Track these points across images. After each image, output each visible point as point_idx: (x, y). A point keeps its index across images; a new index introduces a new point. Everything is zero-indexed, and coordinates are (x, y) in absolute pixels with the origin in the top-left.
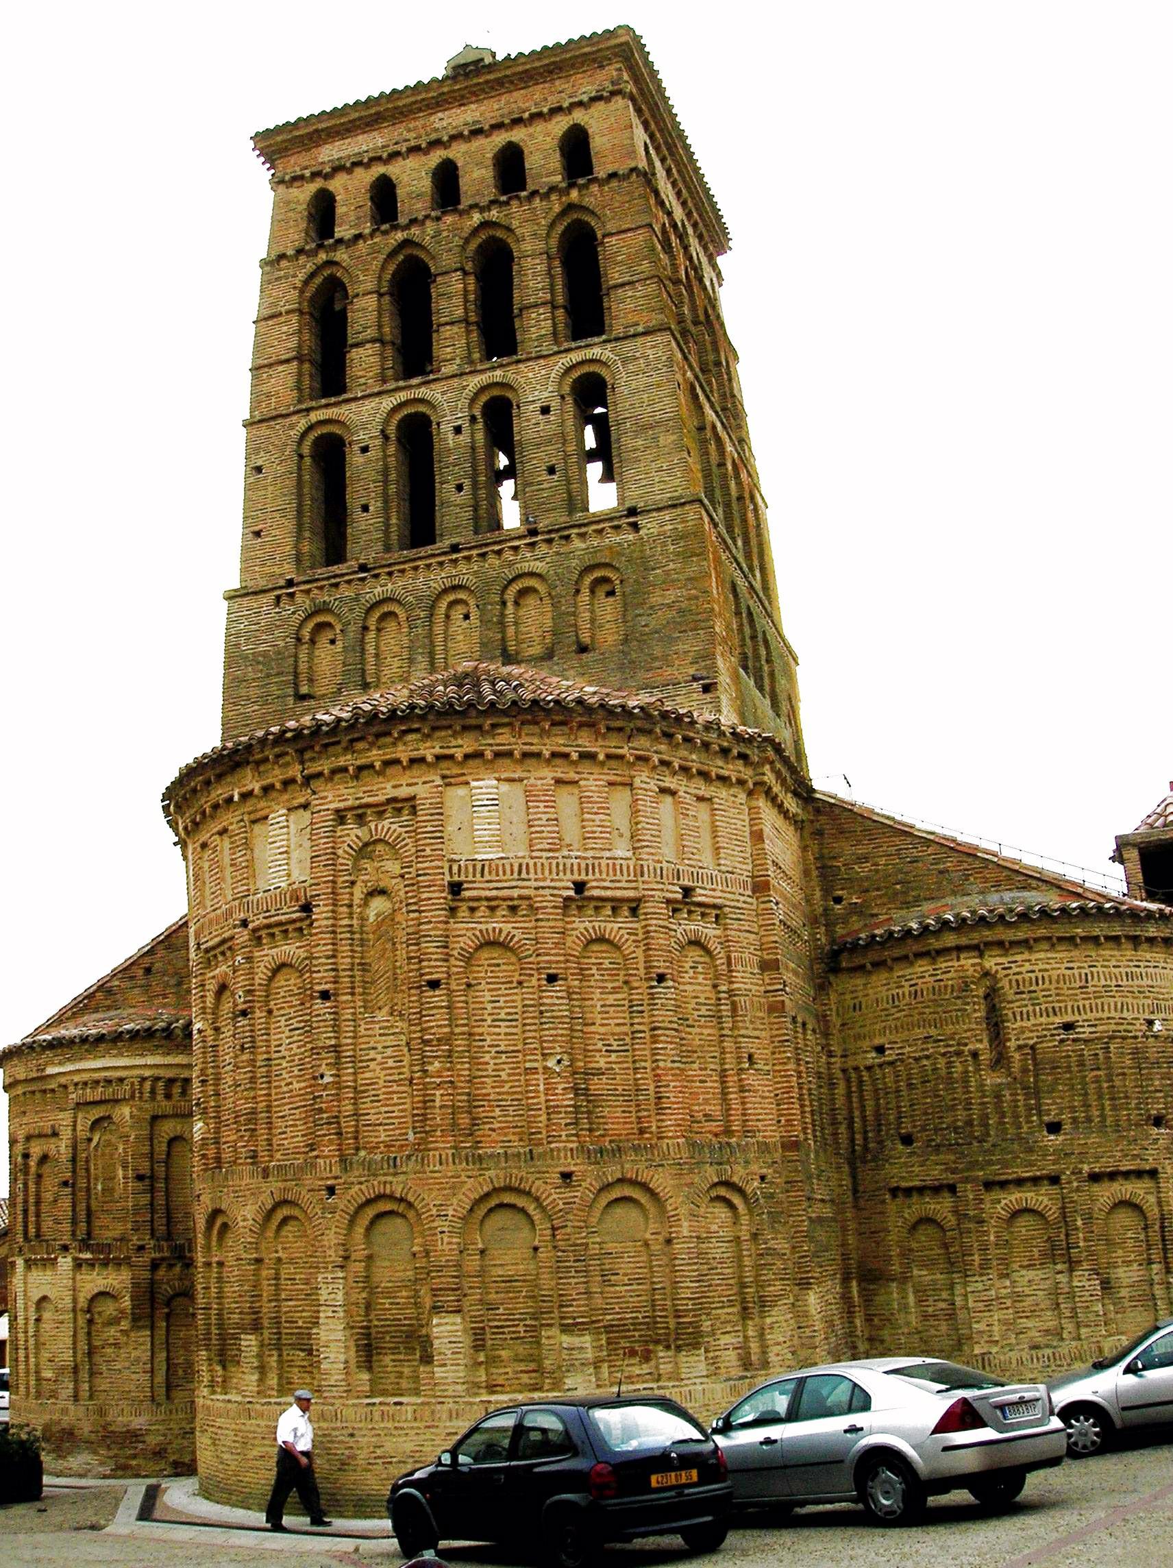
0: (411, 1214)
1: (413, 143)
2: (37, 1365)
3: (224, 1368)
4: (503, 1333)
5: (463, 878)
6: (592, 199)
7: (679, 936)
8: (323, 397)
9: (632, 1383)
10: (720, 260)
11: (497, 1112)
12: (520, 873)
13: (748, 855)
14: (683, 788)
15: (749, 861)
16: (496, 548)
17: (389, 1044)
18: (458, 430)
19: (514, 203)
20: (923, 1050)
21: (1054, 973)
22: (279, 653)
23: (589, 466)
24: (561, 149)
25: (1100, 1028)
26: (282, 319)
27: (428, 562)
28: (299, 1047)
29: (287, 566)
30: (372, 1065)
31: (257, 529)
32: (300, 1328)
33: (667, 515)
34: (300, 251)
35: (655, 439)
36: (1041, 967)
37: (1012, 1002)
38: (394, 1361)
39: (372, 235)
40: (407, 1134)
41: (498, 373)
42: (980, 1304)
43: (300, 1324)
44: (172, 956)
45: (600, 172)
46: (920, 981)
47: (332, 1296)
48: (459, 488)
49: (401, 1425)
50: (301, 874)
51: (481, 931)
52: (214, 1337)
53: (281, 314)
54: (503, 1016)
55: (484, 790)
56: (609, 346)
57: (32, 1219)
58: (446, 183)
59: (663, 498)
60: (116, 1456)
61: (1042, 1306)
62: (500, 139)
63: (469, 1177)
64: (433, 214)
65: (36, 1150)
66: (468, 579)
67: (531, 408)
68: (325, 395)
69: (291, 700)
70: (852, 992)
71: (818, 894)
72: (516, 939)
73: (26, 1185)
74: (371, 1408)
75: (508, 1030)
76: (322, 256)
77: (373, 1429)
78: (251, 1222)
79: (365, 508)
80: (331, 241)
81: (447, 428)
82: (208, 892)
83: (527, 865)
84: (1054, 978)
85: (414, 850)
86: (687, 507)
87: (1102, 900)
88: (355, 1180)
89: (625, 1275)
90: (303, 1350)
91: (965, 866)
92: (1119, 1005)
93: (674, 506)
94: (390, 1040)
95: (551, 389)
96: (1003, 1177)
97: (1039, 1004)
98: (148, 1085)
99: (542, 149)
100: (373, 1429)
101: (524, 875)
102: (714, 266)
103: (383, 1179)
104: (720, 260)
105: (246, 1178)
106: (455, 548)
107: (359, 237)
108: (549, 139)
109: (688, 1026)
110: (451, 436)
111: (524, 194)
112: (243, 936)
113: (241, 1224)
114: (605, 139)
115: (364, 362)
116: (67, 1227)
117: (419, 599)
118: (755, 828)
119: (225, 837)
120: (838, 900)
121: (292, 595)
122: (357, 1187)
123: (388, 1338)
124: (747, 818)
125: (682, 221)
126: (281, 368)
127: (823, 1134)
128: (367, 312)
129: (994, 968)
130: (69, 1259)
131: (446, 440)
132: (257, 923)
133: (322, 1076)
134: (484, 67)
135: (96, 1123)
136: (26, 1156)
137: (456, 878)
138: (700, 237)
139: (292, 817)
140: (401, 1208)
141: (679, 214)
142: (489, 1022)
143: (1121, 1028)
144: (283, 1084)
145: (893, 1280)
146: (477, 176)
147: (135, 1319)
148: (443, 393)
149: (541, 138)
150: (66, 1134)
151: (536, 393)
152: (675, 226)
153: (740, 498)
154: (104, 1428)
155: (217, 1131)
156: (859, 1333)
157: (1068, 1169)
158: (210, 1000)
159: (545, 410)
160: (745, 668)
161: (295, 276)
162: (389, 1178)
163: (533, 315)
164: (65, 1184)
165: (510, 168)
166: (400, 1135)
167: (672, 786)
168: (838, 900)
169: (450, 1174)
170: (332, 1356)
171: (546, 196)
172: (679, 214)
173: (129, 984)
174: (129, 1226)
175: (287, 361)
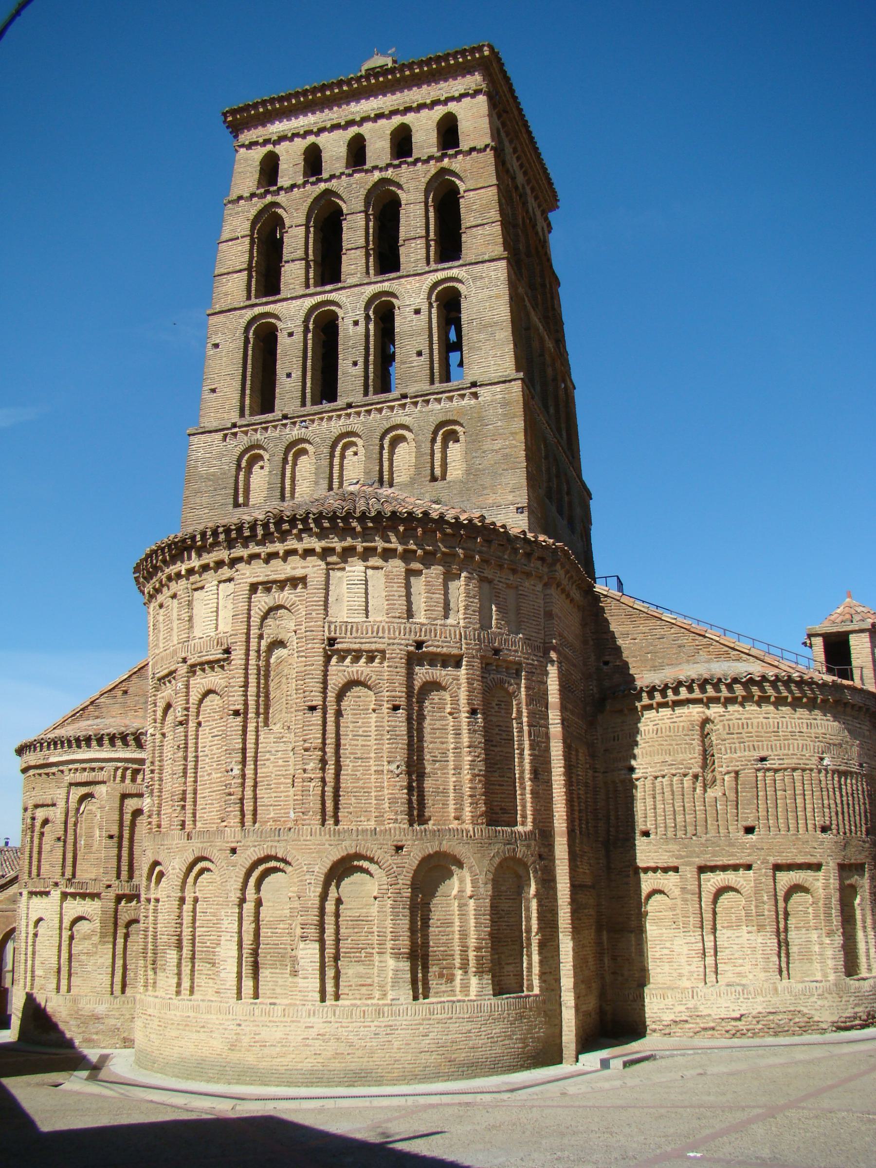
0: (289, 869)
1: (335, 122)
2: (33, 966)
3: (155, 973)
4: (350, 957)
5: (338, 635)
6: (458, 165)
7: (489, 682)
8: (266, 296)
9: (440, 997)
10: (551, 216)
11: (353, 800)
12: (377, 633)
13: (542, 628)
14: (498, 579)
15: (543, 632)
16: (378, 406)
17: (279, 749)
18: (356, 323)
19: (404, 166)
20: (661, 770)
21: (755, 721)
22: (225, 474)
23: (450, 354)
24: (438, 129)
25: (786, 761)
26: (239, 241)
27: (330, 414)
28: (218, 749)
29: (233, 414)
30: (267, 763)
31: (213, 387)
32: (208, 947)
33: (498, 388)
34: (253, 195)
35: (493, 334)
36: (747, 716)
37: (725, 740)
38: (272, 973)
39: (305, 183)
40: (289, 813)
41: (386, 284)
42: (693, 952)
43: (208, 944)
44: (141, 683)
45: (464, 146)
46: (660, 722)
47: (231, 925)
48: (355, 364)
49: (273, 1019)
50: (225, 626)
51: (348, 672)
52: (149, 951)
53: (238, 238)
54: (361, 733)
55: (356, 574)
56: (464, 268)
57: (35, 863)
58: (357, 153)
59: (494, 376)
60: (84, 1032)
61: (736, 956)
62: (397, 120)
63: (331, 845)
64: (347, 171)
65: (41, 814)
66: (357, 428)
67: (408, 310)
68: (266, 295)
69: (231, 507)
70: (613, 728)
71: (593, 658)
72: (373, 679)
73: (32, 837)
74: (253, 1006)
75: (364, 743)
76: (269, 198)
77: (254, 1021)
78: (178, 870)
79: (289, 375)
80: (275, 188)
81: (349, 322)
82: (161, 638)
83: (383, 627)
84: (755, 724)
85: (304, 613)
86: (513, 383)
87: (792, 671)
88: (251, 844)
89: (438, 920)
90: (210, 963)
91: (697, 643)
92: (800, 746)
93: (504, 382)
94: (282, 746)
95: (422, 297)
96: (712, 863)
97: (744, 742)
98: (119, 772)
99: (424, 129)
100: (254, 1021)
101: (380, 634)
102: (546, 219)
103: (270, 844)
104: (551, 216)
105: (176, 839)
106: (349, 406)
107: (293, 186)
108: (430, 122)
109: (492, 746)
110: (351, 327)
111: (410, 160)
112: (183, 669)
113: (171, 872)
114: (469, 123)
115: (293, 273)
116: (59, 870)
117: (324, 440)
118: (547, 609)
119: (175, 601)
120: (606, 663)
121: (235, 434)
122: (253, 849)
123: (269, 958)
124: (542, 602)
125: (523, 185)
126: (235, 275)
127: (587, 827)
128: (296, 240)
129: (713, 715)
130: (59, 892)
131: (347, 329)
132: (193, 660)
133: (232, 770)
134: (386, 69)
135: (83, 798)
136: (33, 819)
137: (333, 634)
138: (536, 198)
139: (222, 586)
140: (282, 865)
141: (520, 179)
142: (350, 737)
143: (801, 761)
144: (205, 774)
145: (631, 932)
146: (379, 147)
147: (103, 935)
148: (348, 297)
149: (424, 121)
150: (61, 804)
151: (412, 299)
152: (516, 188)
153: (555, 379)
154: (77, 1012)
155: (160, 806)
156: (606, 968)
157: (759, 859)
158: (159, 713)
159: (417, 312)
160: (550, 498)
161: (248, 211)
162: (275, 844)
163: (413, 245)
164: (59, 839)
165: (402, 144)
166: (285, 813)
167: (490, 577)
168: (606, 663)
169: (317, 842)
170: (228, 967)
171: (427, 161)
172: (520, 179)
173: (111, 701)
174: (102, 870)
175: (240, 271)
